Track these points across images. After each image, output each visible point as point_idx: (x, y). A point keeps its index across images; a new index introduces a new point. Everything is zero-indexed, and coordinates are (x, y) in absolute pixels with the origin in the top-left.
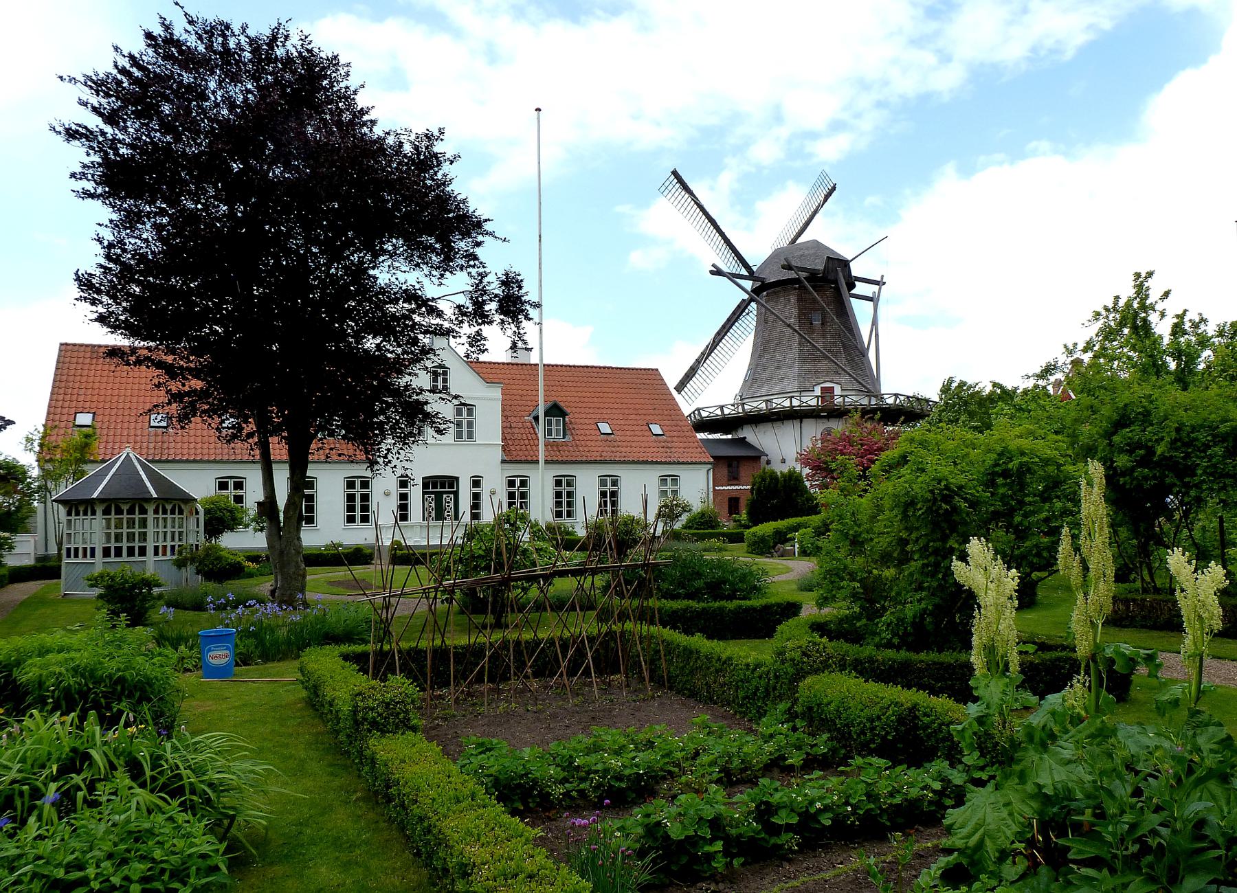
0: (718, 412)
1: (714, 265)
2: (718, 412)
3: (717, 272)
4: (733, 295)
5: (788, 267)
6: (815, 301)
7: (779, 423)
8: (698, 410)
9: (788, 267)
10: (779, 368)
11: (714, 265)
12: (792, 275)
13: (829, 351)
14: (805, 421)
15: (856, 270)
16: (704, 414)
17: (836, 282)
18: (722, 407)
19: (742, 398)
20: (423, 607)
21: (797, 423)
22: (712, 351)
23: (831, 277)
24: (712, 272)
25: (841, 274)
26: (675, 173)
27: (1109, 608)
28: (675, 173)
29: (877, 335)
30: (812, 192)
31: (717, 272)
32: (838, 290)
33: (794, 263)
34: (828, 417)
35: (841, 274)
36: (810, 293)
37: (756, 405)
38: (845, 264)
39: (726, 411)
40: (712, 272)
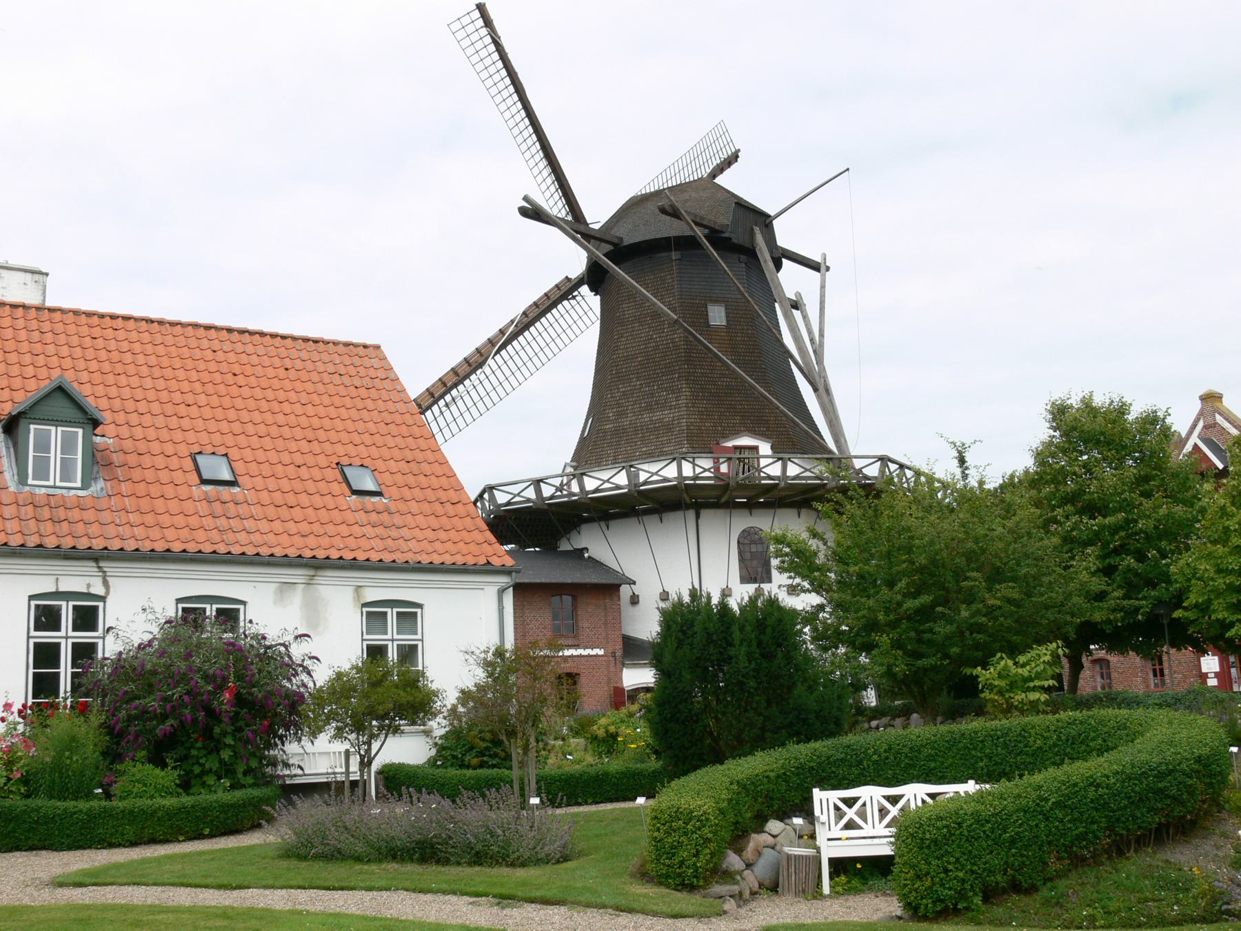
0: (531, 493)
1: (526, 199)
2: (531, 493)
3: (533, 212)
4: (575, 260)
5: (674, 213)
7: (651, 520)
8: (490, 489)
9: (674, 213)
11: (526, 199)
14: (705, 513)
15: (786, 235)
16: (501, 498)
18: (537, 483)
19: (589, 452)
20: (678, 336)
21: (691, 514)
26: (481, 8)
27: (1205, 751)
28: (481, 8)
34: (751, 506)
37: (608, 480)
38: (764, 221)
39: (547, 491)
40: (524, 212)
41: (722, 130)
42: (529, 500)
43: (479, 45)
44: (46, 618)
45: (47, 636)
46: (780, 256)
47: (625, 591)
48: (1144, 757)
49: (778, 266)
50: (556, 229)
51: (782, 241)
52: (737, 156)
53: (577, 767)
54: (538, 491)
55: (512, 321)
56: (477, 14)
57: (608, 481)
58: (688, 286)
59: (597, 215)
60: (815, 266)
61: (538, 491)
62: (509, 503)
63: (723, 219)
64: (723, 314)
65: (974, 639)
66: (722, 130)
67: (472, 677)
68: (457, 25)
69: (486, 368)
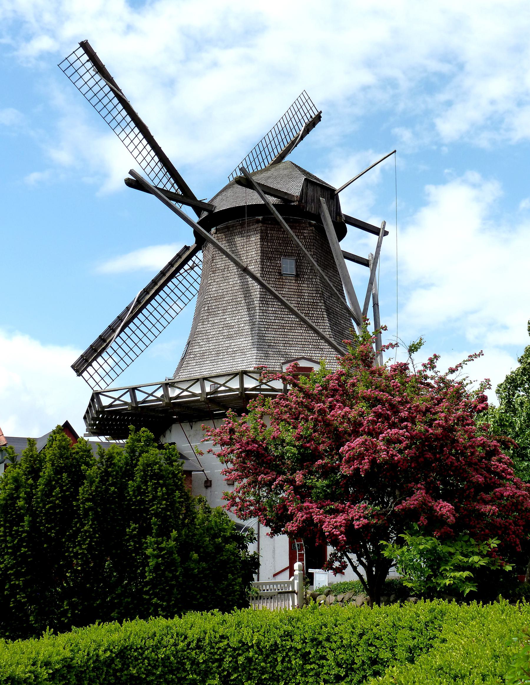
0: (127, 398)
2: (127, 398)
3: (136, 183)
6: (287, 241)
10: (230, 337)
11: (131, 172)
12: (253, 198)
13: (307, 314)
14: (245, 266)
17: (318, 217)
18: (133, 390)
19: (175, 377)
22: (112, 329)
23: (311, 208)
24: (129, 183)
25: (325, 207)
29: (376, 305)
30: (113, 125)
31: (136, 183)
32: (321, 231)
33: (256, 179)
35: (325, 207)
36: (285, 232)
39: (140, 397)
40: (129, 183)
41: (304, 98)
42: (126, 403)
43: (105, 101)
46: (342, 224)
49: (341, 234)
50: (153, 197)
51: (346, 210)
52: (320, 117)
53: (197, 389)
54: (133, 397)
55: (128, 308)
56: (81, 51)
57: (186, 390)
60: (375, 231)
61: (133, 397)
62: (111, 406)
64: (294, 266)
65: (280, 498)
66: (304, 98)
69: (109, 350)
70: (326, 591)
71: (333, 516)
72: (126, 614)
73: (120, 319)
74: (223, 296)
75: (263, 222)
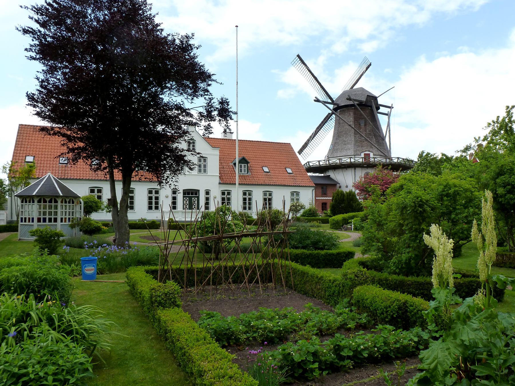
0: (318, 164)
1: (316, 98)
2: (318, 164)
3: (317, 100)
7: (345, 169)
10: (345, 144)
11: (316, 98)
12: (351, 103)
13: (368, 137)
15: (380, 101)
17: (371, 107)
18: (319, 161)
19: (328, 158)
23: (369, 104)
24: (315, 101)
29: (389, 131)
32: (372, 110)
33: (352, 98)
38: (375, 98)
39: (321, 163)
40: (315, 101)
44: (150, 192)
45: (150, 195)
47: (338, 185)
48: (334, 235)
54: (319, 163)
58: (359, 113)
59: (335, 97)
61: (319, 163)
63: (364, 99)
67: (163, 318)
68: (293, 62)
70: (343, 330)
71: (434, 259)
72: (352, 212)
73: (311, 137)
74: (342, 132)
75: (354, 109)
